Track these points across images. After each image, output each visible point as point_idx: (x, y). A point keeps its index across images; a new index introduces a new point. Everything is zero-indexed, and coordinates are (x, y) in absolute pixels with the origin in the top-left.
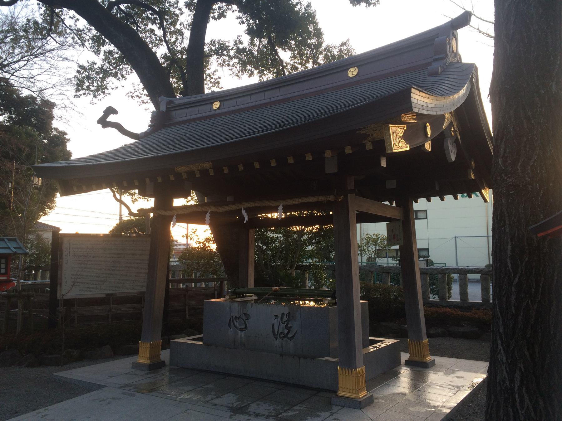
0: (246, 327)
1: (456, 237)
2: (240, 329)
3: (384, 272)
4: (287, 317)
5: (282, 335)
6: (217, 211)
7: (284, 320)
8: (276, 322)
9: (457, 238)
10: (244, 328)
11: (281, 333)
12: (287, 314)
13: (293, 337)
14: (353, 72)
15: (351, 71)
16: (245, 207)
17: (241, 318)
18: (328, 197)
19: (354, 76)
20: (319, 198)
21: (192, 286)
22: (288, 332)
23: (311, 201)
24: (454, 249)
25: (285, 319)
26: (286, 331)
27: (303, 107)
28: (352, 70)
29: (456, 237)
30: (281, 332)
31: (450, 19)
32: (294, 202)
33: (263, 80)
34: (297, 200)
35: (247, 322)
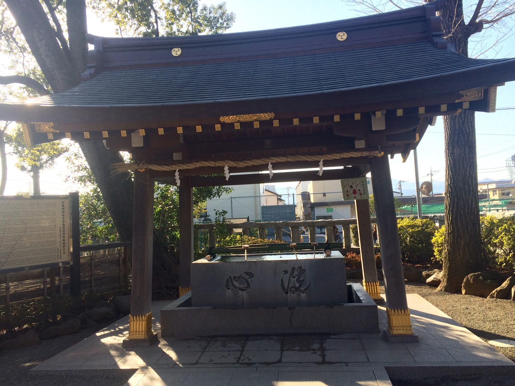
0: (249, 285)
1: (231, 198)
2: (240, 288)
3: (261, 228)
4: (298, 271)
5: (293, 289)
6: (237, 166)
7: (295, 274)
8: (286, 277)
9: (232, 199)
10: (246, 287)
11: (291, 287)
12: (298, 269)
13: (306, 289)
14: (176, 51)
15: (175, 50)
16: (274, 162)
17: (242, 277)
18: (373, 152)
19: (176, 55)
20: (363, 153)
21: (109, 250)
22: (300, 286)
23: (354, 156)
24: (230, 208)
25: (296, 273)
26: (297, 285)
27: (323, 68)
28: (176, 49)
29: (231, 198)
30: (292, 285)
31: (397, 9)
32: (334, 158)
33: (484, 24)
34: (338, 155)
35: (250, 280)
